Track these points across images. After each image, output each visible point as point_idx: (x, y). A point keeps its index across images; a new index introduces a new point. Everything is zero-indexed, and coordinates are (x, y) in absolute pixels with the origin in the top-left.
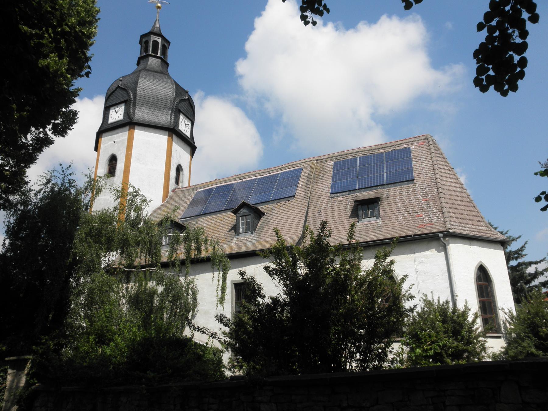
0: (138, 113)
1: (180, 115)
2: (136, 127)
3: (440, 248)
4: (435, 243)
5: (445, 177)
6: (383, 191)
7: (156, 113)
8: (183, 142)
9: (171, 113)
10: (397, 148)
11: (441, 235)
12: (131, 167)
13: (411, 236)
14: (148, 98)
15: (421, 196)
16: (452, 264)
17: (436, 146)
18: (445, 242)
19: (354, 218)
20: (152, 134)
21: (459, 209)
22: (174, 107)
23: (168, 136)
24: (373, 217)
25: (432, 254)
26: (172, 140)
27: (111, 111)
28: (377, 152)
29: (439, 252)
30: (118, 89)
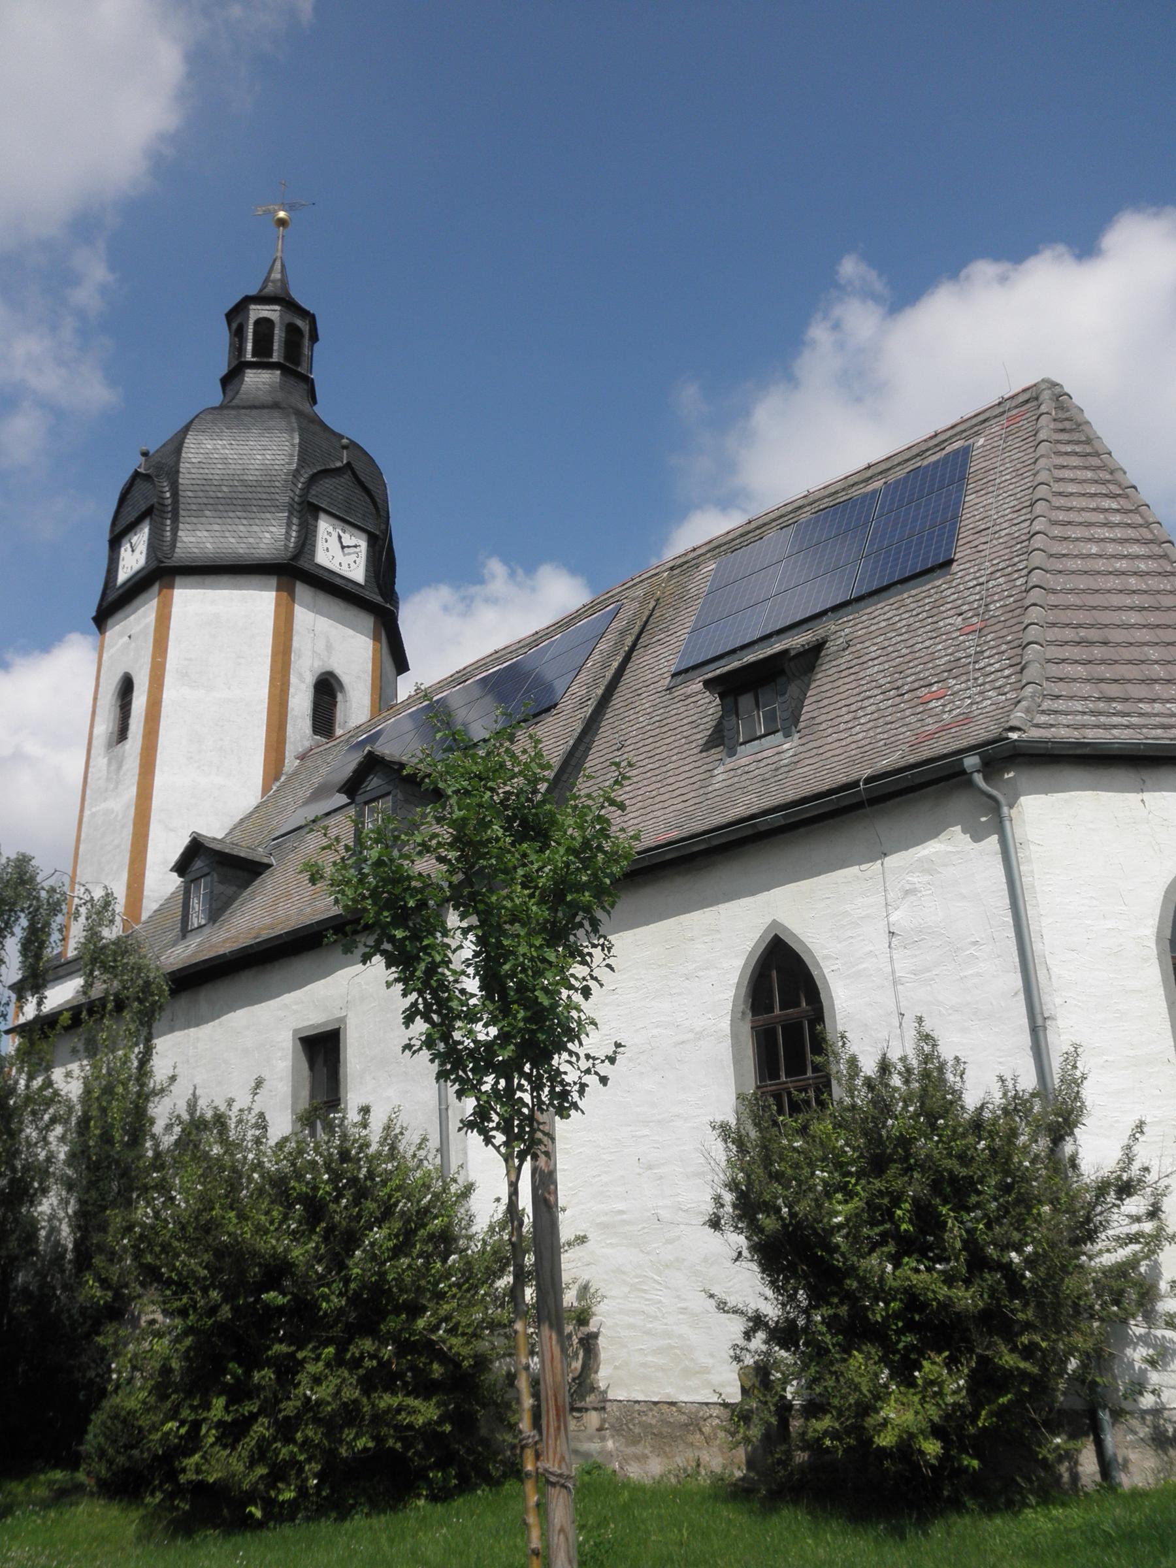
0: (185, 539)
1: (316, 519)
2: (178, 580)
3: (983, 819)
4: (960, 802)
5: (1080, 524)
6: (837, 628)
7: (242, 528)
8: (338, 601)
9: (288, 517)
10: (926, 463)
11: (971, 762)
12: (164, 704)
13: (856, 784)
14: (214, 488)
15: (960, 618)
16: (1033, 886)
17: (1067, 415)
18: (994, 792)
19: (713, 751)
20: (226, 592)
21: (1118, 644)
22: (297, 499)
23: (278, 589)
24: (774, 733)
25: (950, 849)
26: (293, 601)
27: (123, 549)
28: (855, 492)
29: (977, 838)
30: (138, 480)
